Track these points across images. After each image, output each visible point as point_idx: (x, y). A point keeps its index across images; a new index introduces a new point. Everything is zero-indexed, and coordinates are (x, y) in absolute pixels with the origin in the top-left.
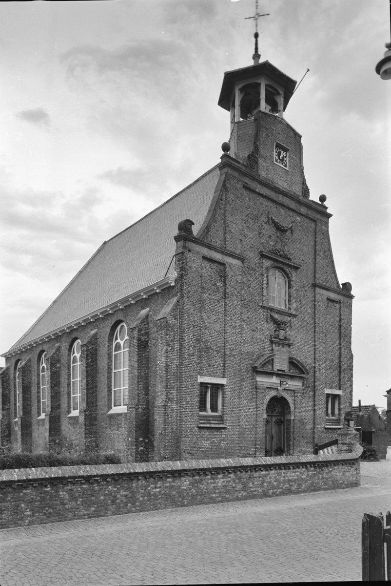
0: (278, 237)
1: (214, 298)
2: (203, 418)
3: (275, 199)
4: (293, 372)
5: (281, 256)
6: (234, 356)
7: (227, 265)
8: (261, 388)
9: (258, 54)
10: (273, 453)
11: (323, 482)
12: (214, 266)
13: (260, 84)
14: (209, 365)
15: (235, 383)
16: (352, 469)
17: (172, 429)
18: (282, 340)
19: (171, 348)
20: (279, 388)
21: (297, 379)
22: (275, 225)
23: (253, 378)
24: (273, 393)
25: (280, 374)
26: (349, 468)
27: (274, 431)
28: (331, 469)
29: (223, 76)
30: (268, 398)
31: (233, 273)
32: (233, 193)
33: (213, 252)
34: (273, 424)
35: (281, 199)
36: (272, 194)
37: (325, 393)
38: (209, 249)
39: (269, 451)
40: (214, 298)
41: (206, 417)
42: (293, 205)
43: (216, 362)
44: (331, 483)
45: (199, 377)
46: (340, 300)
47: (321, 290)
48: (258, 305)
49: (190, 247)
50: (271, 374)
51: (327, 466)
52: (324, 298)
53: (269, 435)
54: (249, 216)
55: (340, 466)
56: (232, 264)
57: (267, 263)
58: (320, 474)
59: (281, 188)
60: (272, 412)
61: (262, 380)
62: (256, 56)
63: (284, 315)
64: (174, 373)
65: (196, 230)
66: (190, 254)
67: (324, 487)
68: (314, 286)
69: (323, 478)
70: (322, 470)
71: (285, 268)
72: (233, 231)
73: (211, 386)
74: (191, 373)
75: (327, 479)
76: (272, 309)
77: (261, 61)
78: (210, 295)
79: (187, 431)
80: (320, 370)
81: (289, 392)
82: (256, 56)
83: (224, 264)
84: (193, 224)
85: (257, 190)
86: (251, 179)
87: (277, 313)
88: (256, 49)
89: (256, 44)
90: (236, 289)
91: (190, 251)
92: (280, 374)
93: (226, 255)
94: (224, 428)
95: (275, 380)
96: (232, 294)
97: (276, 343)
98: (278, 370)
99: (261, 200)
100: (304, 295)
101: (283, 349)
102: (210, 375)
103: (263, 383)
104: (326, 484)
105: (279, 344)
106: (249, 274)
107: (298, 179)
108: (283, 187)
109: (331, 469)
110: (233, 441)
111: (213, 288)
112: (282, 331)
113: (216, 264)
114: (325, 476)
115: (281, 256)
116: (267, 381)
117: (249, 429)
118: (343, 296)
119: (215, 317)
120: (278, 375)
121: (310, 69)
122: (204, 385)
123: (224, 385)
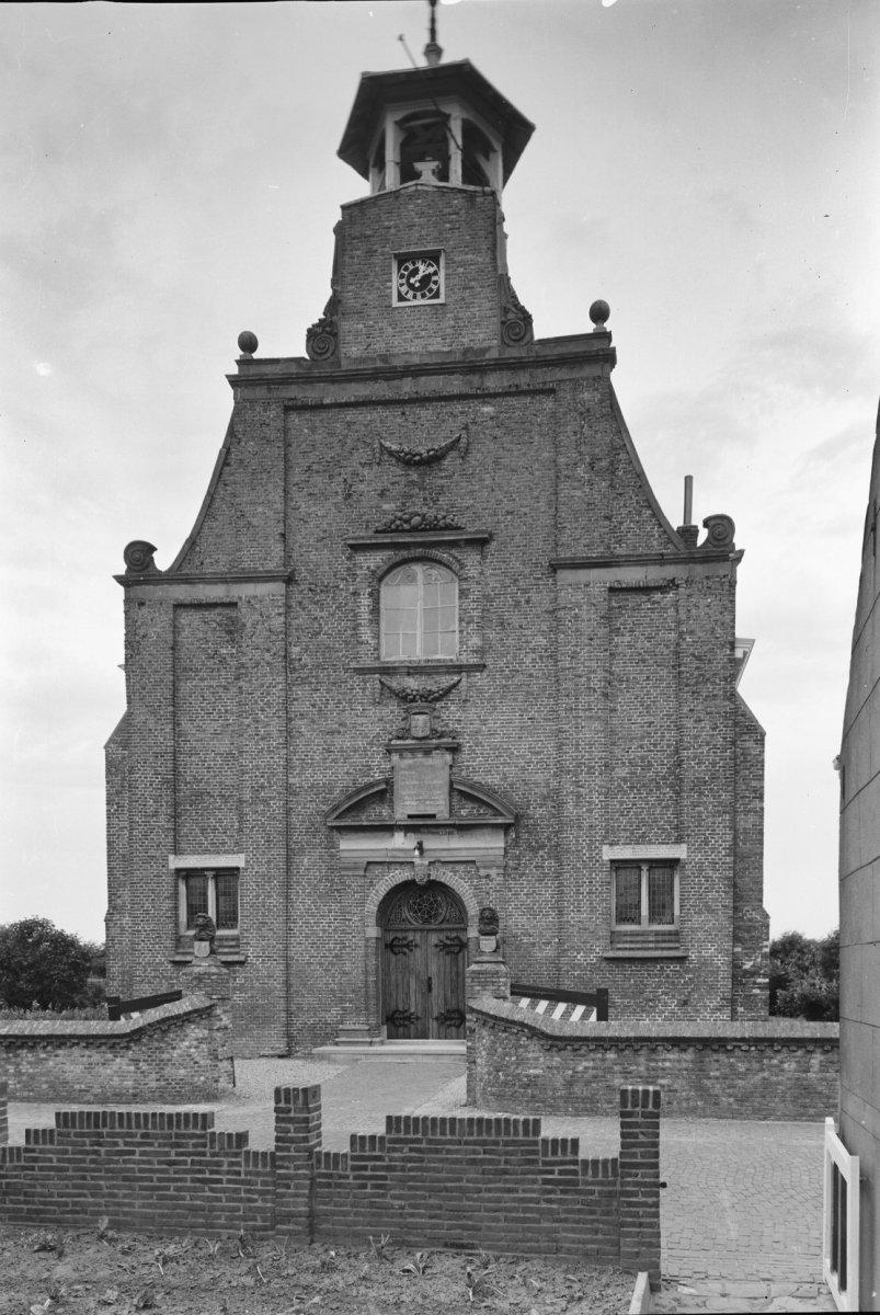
0: (412, 483)
1: (214, 683)
2: (667, 938)
3: (389, 395)
4: (466, 812)
5: (415, 529)
6: (265, 801)
7: (240, 604)
8: (353, 865)
9: (435, 45)
10: (433, 1025)
11: (19, 1083)
12: (212, 615)
13: (448, 117)
14: (203, 830)
15: (269, 862)
16: (118, 1060)
17: (123, 965)
18: (424, 738)
19: (115, 807)
20: (417, 861)
21: (485, 831)
22: (399, 459)
23: (332, 845)
24: (400, 876)
25: (421, 825)
26: (110, 1056)
27: (433, 969)
28: (43, 1056)
29: (341, 163)
30: (382, 889)
31: (256, 617)
32: (253, 439)
33: (201, 586)
34: (432, 950)
35: (407, 387)
36: (380, 389)
37: (606, 857)
38: (190, 583)
39: (417, 1018)
40: (214, 683)
41: (637, 935)
42: (456, 384)
43: (220, 821)
44: (45, 1086)
45: (171, 857)
46: (673, 581)
47: (586, 572)
48: (346, 671)
49: (140, 595)
50: (388, 829)
51: (32, 1048)
52: (598, 591)
53: (417, 977)
54: (315, 467)
55: (76, 1051)
56: (255, 597)
57: (375, 560)
58: (10, 1064)
59: (427, 360)
60: (426, 921)
61: (355, 847)
62: (433, 49)
63: (438, 673)
64: (124, 856)
65: (164, 561)
66: (144, 610)
67: (25, 1094)
68: (555, 567)
69: (19, 1074)
70: (17, 1056)
71: (434, 553)
72: (256, 524)
73: (212, 873)
74: (152, 852)
75: (32, 1077)
76: (388, 670)
77: (446, 59)
78: (202, 679)
79: (146, 970)
80: (579, 796)
81: (461, 868)
82: (433, 49)
83: (233, 605)
84: (154, 549)
85: (327, 401)
86: (303, 383)
87: (409, 674)
88: (433, 32)
89: (433, 20)
90: (268, 651)
91: (142, 604)
92: (421, 825)
93: (236, 582)
94: (241, 963)
95: (401, 842)
96: (257, 664)
97: (401, 751)
98: (410, 817)
99: (350, 415)
100: (517, 604)
101: (429, 761)
102: (206, 851)
103: (359, 854)
104: (26, 1087)
105: (412, 751)
106: (316, 603)
107: (484, 305)
108: (431, 353)
109: (43, 1056)
110: (267, 992)
111: (210, 663)
112: (416, 717)
113: (218, 610)
114: (25, 1068)
115: (415, 529)
116: (373, 847)
117: (321, 964)
118: (687, 563)
119: (215, 725)
120: (407, 829)
121: (397, 34)
122: (187, 874)
123: (238, 869)
